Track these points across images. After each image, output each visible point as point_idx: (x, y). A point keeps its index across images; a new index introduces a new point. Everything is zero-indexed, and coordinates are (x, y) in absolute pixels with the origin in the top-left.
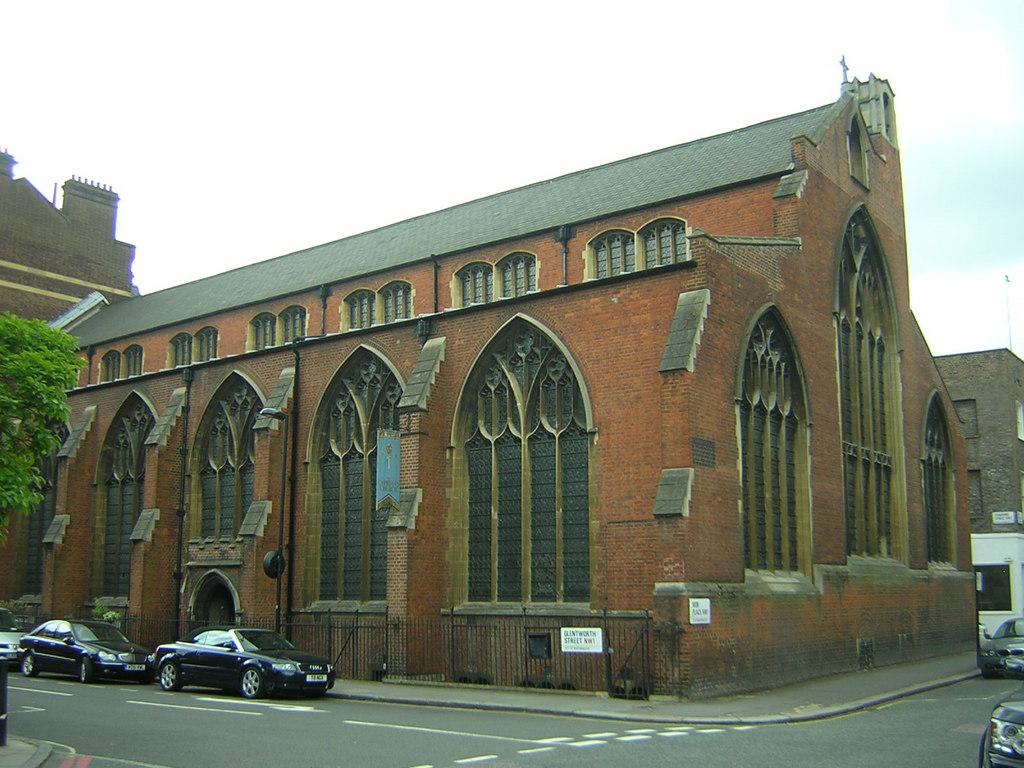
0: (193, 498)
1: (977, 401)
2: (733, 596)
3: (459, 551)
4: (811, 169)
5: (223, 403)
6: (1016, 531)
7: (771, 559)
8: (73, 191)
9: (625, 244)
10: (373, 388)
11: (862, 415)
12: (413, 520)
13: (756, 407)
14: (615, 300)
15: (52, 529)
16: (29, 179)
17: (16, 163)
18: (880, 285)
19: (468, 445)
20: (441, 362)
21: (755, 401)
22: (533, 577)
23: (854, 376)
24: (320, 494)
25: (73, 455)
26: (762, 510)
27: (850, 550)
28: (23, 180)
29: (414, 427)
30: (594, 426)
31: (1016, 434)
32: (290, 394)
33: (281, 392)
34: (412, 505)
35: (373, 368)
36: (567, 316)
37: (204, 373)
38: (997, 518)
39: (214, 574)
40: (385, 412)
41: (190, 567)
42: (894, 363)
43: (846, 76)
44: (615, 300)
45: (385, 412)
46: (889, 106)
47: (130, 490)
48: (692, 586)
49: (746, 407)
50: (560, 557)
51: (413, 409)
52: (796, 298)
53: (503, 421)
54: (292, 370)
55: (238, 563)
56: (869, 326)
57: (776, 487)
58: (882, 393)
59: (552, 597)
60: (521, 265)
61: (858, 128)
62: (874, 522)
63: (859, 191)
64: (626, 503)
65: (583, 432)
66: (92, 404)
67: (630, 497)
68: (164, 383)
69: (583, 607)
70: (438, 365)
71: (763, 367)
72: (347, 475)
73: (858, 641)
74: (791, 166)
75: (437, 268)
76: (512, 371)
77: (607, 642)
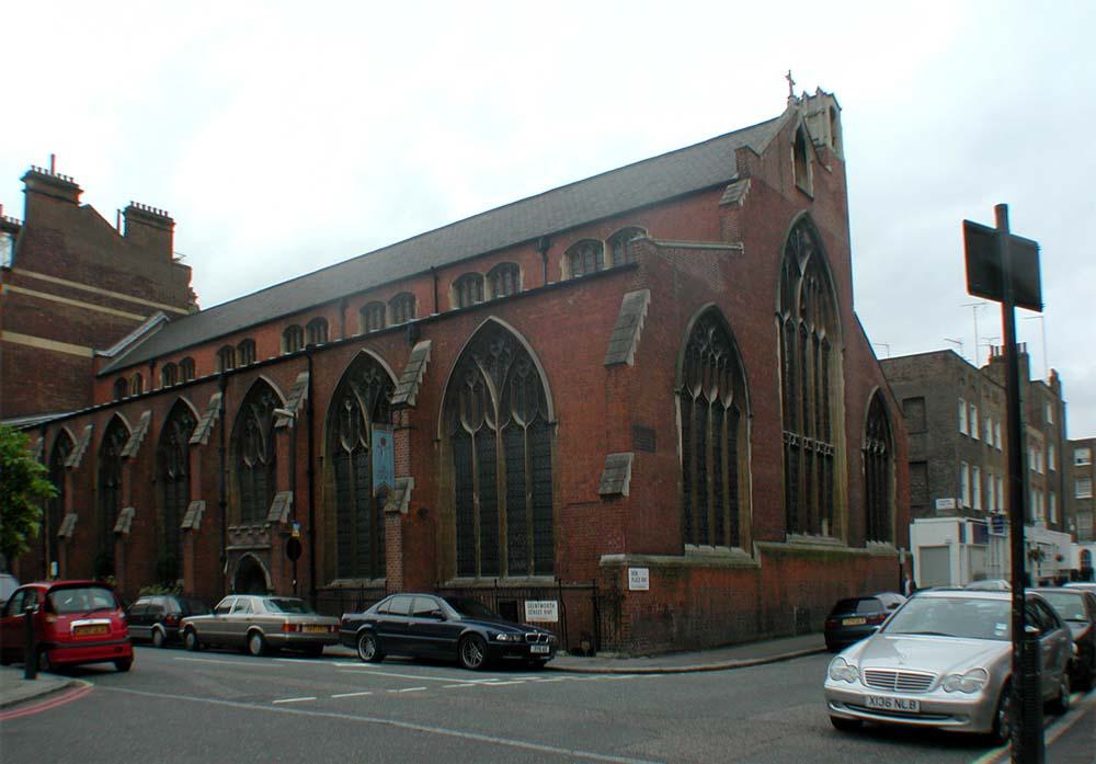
0: (232, 490)
1: (926, 399)
2: (674, 568)
3: (449, 529)
4: (753, 178)
5: (253, 406)
6: (956, 516)
7: (728, 537)
8: (134, 218)
9: (596, 253)
10: (373, 389)
11: (804, 407)
12: (407, 505)
13: (713, 404)
14: (570, 302)
15: (120, 520)
16: (94, 207)
17: (82, 191)
18: (825, 288)
19: (451, 438)
20: (427, 363)
21: (697, 393)
22: (509, 554)
23: (798, 372)
24: (334, 485)
25: (133, 455)
26: (703, 493)
27: (790, 529)
28: (89, 208)
29: (405, 422)
30: (555, 417)
31: (959, 428)
32: (305, 395)
33: (297, 394)
34: (405, 493)
35: (373, 371)
36: (532, 317)
37: (236, 379)
38: (941, 504)
39: (248, 556)
40: (382, 411)
41: (231, 551)
42: (837, 358)
43: (791, 90)
44: (570, 302)
45: (382, 411)
46: (836, 120)
47: (182, 485)
48: (631, 557)
49: (687, 399)
50: (531, 537)
51: (402, 405)
52: (738, 299)
53: (481, 415)
54: (307, 375)
55: (267, 546)
56: (813, 327)
57: (718, 472)
58: (826, 389)
59: (524, 572)
60: (508, 275)
61: (805, 144)
62: (815, 505)
63: (803, 200)
64: (583, 486)
65: (547, 424)
66: (146, 410)
67: (585, 482)
68: (204, 389)
69: (549, 580)
70: (425, 365)
71: (705, 363)
72: (356, 468)
73: (795, 609)
74: (736, 176)
75: (437, 279)
76: (487, 369)
77: (562, 614)
